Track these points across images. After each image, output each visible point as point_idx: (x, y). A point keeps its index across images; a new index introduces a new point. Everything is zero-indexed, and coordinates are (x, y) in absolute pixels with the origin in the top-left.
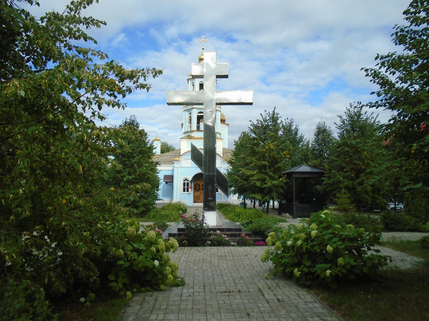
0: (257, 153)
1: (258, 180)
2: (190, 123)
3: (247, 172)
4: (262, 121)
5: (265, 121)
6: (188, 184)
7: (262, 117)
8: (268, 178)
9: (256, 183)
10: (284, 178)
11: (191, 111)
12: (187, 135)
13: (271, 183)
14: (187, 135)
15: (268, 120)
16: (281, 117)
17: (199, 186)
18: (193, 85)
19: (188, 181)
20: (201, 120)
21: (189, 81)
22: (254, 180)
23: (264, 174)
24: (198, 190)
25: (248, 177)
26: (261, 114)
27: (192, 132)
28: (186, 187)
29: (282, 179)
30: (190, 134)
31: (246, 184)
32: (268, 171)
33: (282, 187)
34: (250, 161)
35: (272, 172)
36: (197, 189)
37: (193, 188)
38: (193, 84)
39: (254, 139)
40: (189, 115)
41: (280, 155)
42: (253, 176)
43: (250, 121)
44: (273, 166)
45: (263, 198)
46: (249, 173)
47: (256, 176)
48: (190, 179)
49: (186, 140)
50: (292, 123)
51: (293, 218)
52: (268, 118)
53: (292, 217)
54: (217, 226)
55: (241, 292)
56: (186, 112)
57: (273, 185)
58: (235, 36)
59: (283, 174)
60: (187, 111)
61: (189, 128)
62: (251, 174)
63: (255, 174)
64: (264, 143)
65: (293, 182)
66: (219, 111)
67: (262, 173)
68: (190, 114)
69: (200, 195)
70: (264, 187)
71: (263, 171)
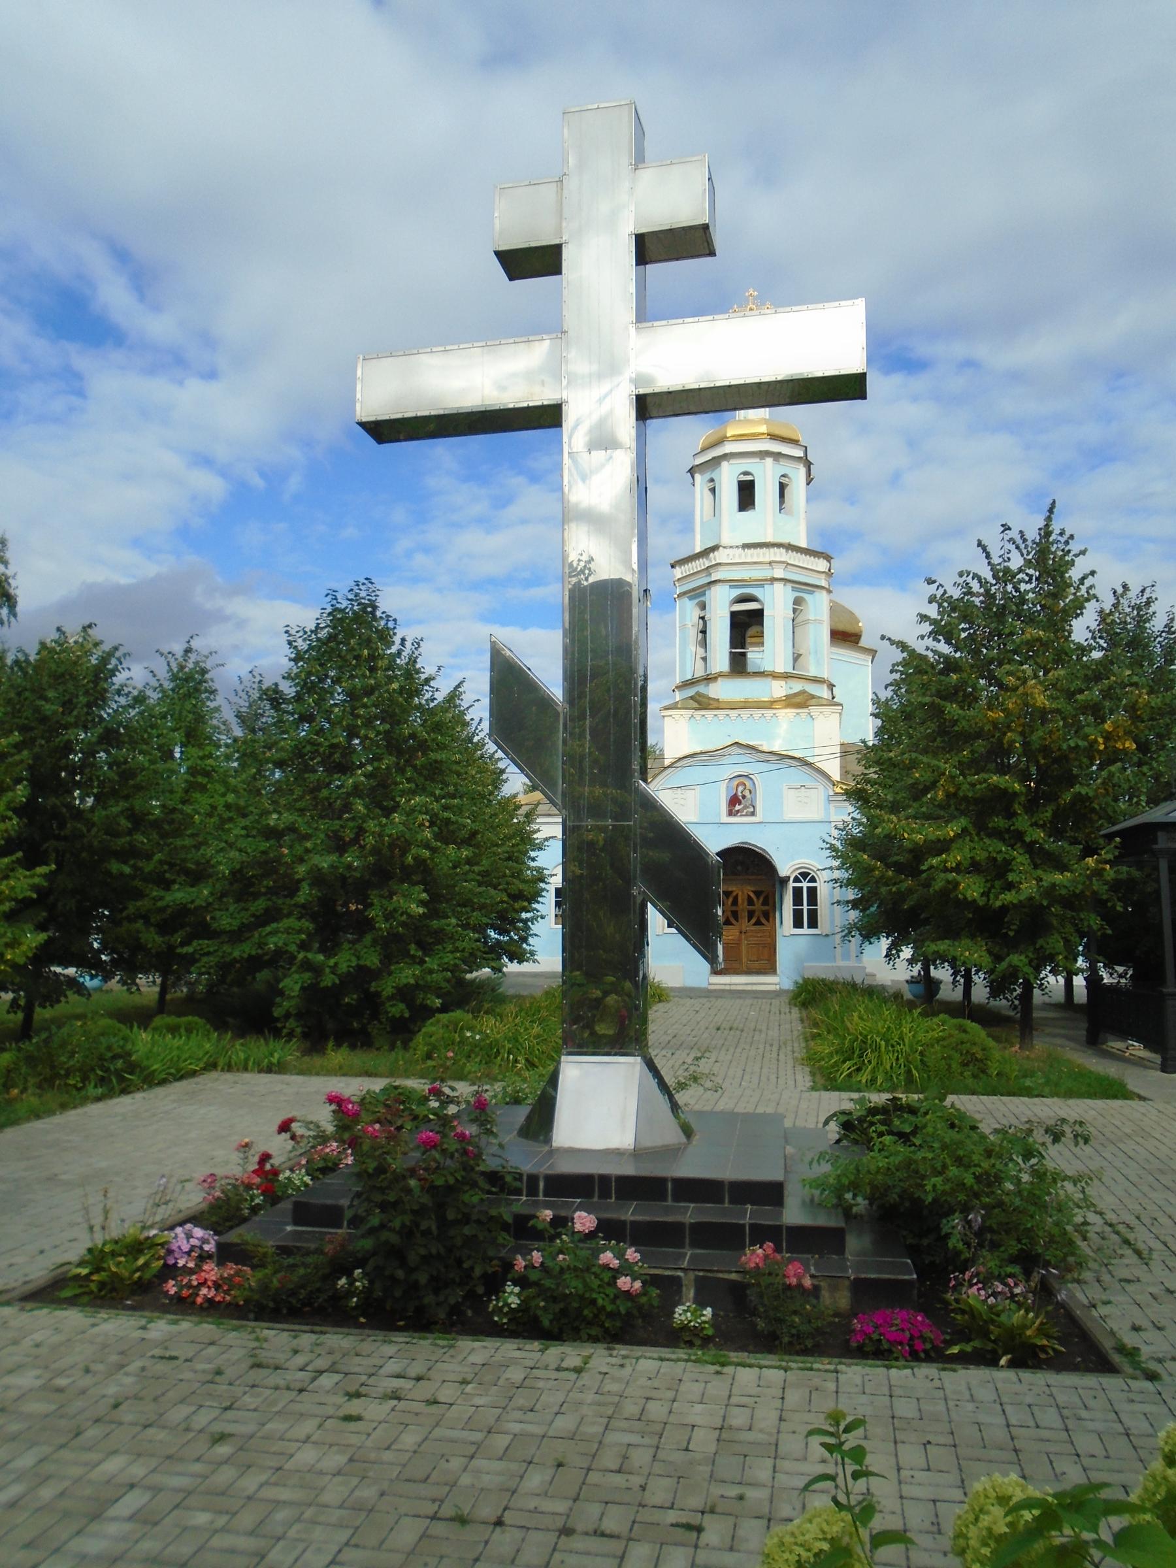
0: (968, 737)
1: (974, 867)
2: (704, 643)
3: (912, 830)
4: (987, 574)
5: (1004, 575)
7: (988, 556)
8: (1020, 859)
9: (957, 884)
10: (1106, 854)
11: (704, 594)
12: (691, 692)
13: (1039, 880)
14: (691, 692)
15: (1020, 570)
16: (1083, 552)
18: (713, 490)
20: (751, 631)
21: (698, 477)
22: (946, 870)
23: (1003, 840)
25: (919, 853)
26: (980, 544)
27: (709, 679)
29: (1098, 862)
30: (701, 689)
31: (910, 891)
32: (1022, 822)
33: (1100, 905)
34: (928, 777)
35: (1043, 826)
38: (711, 485)
39: (950, 665)
40: (697, 613)
41: (1085, 737)
42: (942, 846)
43: (930, 582)
44: (1052, 797)
45: (998, 958)
46: (919, 833)
47: (960, 849)
49: (683, 712)
50: (1149, 603)
51: (1164, 1069)
52: (1016, 562)
53: (1157, 1058)
54: (637, 1154)
56: (686, 600)
57: (1050, 891)
58: (923, 349)
59: (1105, 836)
60: (691, 598)
61: (700, 663)
62: (932, 837)
63: (952, 840)
64: (1001, 686)
65: (1157, 881)
66: (823, 588)
67: (989, 836)
68: (703, 606)
69: (740, 939)
70: (998, 904)
71: (998, 822)
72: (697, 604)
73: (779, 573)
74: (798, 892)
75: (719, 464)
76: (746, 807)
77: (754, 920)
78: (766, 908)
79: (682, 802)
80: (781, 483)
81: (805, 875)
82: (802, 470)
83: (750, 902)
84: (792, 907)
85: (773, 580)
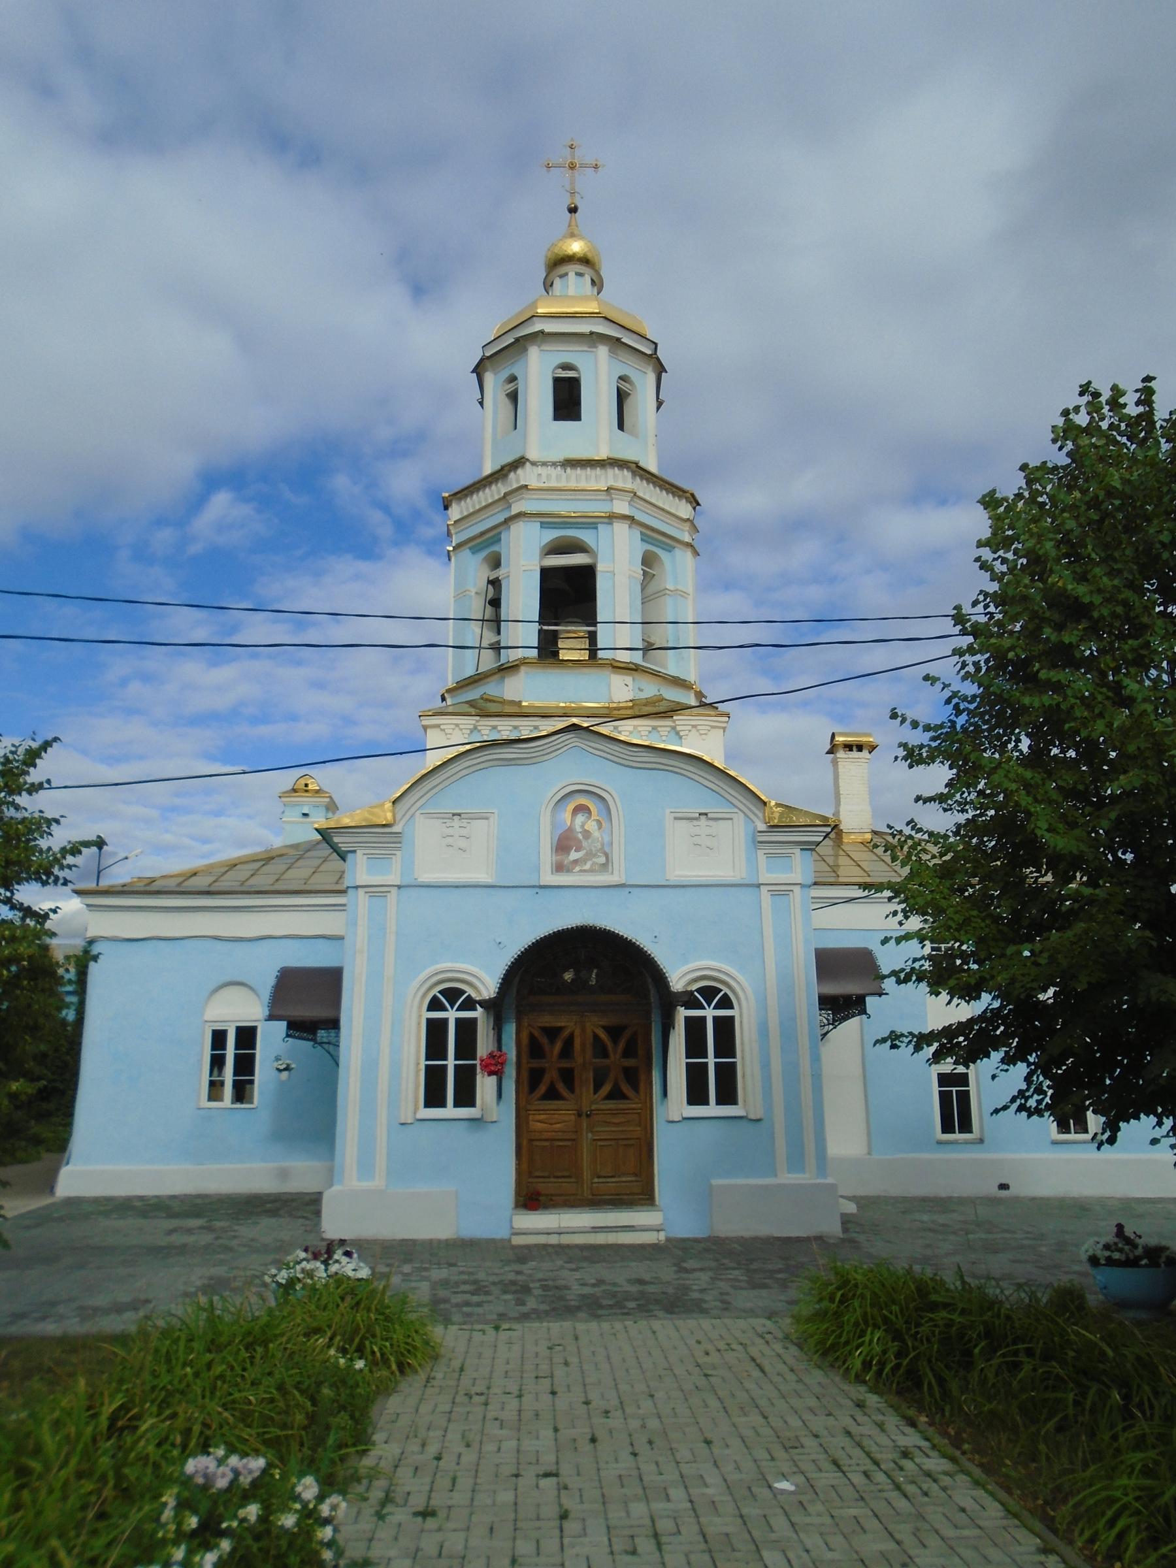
6: (467, 1029)
11: (497, 540)
12: (474, 694)
17: (567, 1050)
18: (513, 397)
19: (469, 1004)
21: (489, 378)
24: (561, 1088)
28: (451, 1062)
30: (490, 689)
36: (551, 1075)
37: (510, 1072)
38: (510, 387)
40: (485, 574)
48: (487, 985)
55: (593, 1435)
56: (466, 553)
60: (475, 550)
68: (496, 562)
72: (486, 559)
73: (621, 507)
74: (695, 1028)
75: (525, 350)
76: (590, 855)
77: (606, 1089)
78: (631, 1062)
79: (462, 843)
80: (618, 389)
81: (709, 993)
82: (651, 377)
83: (601, 1050)
84: (684, 1061)
85: (612, 517)
